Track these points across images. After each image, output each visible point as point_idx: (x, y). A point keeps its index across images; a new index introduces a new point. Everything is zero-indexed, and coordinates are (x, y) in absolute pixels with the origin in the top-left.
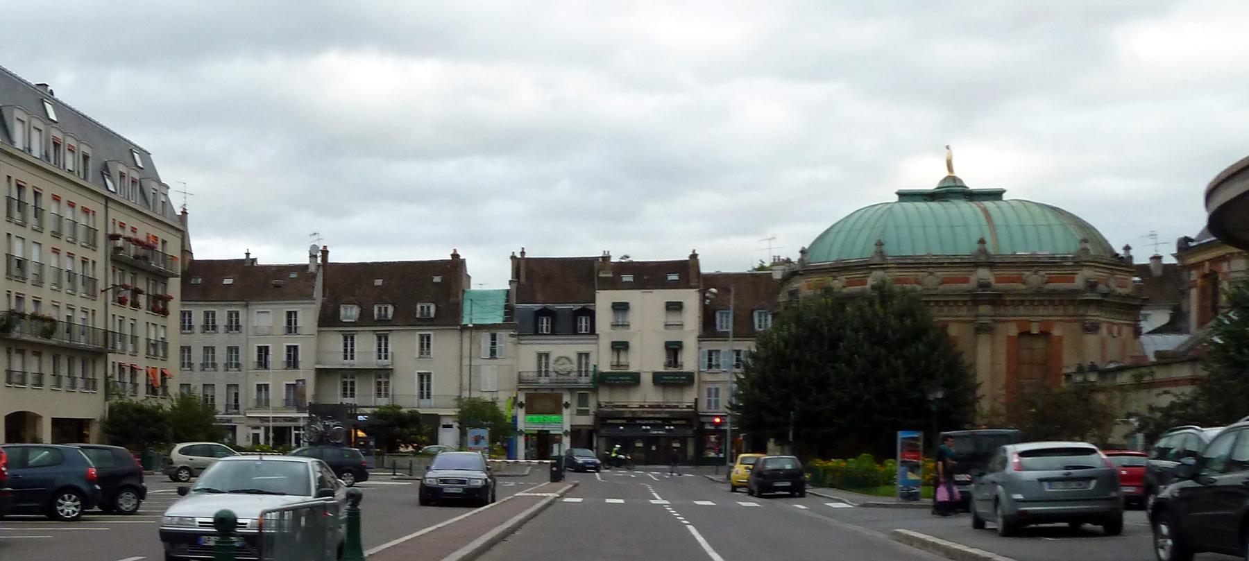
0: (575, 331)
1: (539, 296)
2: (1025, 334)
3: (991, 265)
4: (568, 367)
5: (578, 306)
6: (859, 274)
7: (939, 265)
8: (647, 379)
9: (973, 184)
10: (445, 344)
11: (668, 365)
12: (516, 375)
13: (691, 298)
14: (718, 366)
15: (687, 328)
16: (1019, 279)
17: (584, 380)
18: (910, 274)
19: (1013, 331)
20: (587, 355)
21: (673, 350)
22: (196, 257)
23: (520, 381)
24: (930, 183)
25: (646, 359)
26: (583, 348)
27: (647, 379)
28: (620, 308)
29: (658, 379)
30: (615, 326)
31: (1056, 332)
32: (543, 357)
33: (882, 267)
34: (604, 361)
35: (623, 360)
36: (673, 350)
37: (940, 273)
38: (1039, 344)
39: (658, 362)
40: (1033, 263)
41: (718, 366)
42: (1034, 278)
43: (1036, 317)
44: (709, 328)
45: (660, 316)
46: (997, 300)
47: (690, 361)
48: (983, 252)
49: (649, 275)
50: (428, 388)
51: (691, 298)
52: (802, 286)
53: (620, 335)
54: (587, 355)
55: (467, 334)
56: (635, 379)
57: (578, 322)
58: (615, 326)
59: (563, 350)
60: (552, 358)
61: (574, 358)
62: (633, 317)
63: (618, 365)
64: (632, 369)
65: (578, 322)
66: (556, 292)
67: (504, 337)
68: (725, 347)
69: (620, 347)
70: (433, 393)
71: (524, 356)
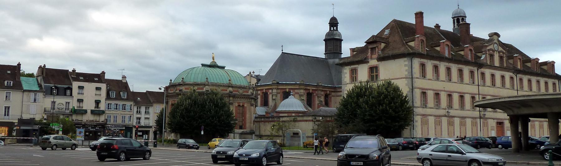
0: (65, 94)
1: (52, 82)
2: (239, 106)
3: (232, 87)
4: (62, 107)
5: (66, 86)
6: (201, 87)
7: (221, 86)
8: (89, 112)
9: (219, 65)
10: (16, 96)
11: (95, 107)
12: (43, 109)
13: (103, 86)
14: (111, 108)
15: (102, 96)
16: (238, 91)
17: (68, 112)
18: (215, 87)
19: (237, 105)
20: (69, 103)
21: (97, 102)
22: (426, 24)
23: (45, 111)
24: (208, 62)
25: (89, 105)
26: (68, 101)
27: (89, 112)
28: (81, 88)
29: (93, 112)
30: (79, 94)
31: (245, 106)
32: (54, 103)
33: (208, 85)
34: (74, 104)
35: (81, 105)
36: (97, 102)
37: (221, 88)
38: (241, 108)
39: (92, 107)
40: (241, 87)
41: (111, 108)
42: (241, 91)
43: (242, 101)
44: (108, 97)
45: (94, 91)
46: (234, 96)
47: (102, 107)
48: (183, 82)
49: (89, 78)
50: (8, 112)
51: (103, 86)
52: (183, 88)
53: (80, 97)
54: (69, 103)
55: (26, 93)
56: (86, 112)
57: (66, 91)
58: (79, 94)
59: (61, 101)
60: (56, 104)
61: (64, 104)
62: (85, 91)
63: (79, 107)
64: (84, 108)
65: (66, 91)
66: (56, 80)
67: (40, 96)
68: (113, 103)
69: (80, 101)
70: (10, 113)
71: (46, 102)
